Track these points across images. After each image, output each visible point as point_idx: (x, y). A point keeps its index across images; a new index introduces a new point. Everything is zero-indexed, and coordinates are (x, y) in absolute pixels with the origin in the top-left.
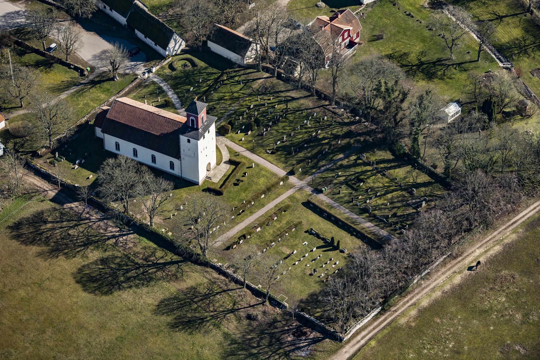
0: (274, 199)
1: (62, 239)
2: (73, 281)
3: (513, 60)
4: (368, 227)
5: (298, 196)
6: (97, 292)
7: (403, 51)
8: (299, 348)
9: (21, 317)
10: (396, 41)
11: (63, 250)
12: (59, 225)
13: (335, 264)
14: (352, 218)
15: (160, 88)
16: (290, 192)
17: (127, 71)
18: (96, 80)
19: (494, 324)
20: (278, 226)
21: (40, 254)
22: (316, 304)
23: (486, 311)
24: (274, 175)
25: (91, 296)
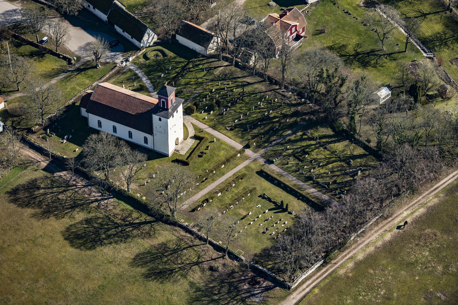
1: (53, 202)
2: (62, 238)
3: (435, 51)
4: (312, 193)
5: (253, 166)
6: (82, 247)
7: (342, 43)
8: (254, 295)
10: (336, 35)
11: (53, 212)
12: (50, 191)
15: (136, 75)
16: (246, 163)
17: (108, 60)
18: (82, 67)
19: (419, 275)
20: (236, 191)
21: (34, 216)
22: (268, 258)
23: (412, 264)
24: (233, 148)
25: (77, 251)
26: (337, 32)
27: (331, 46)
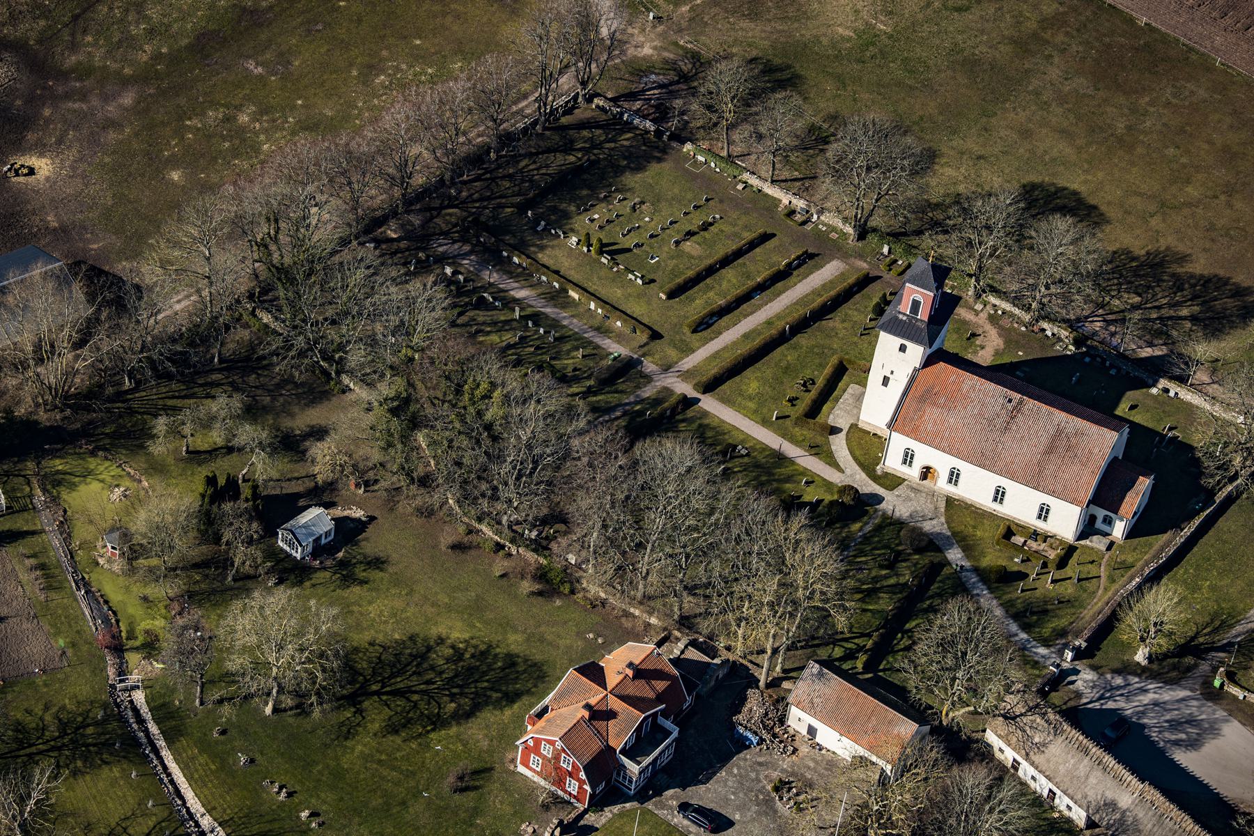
0: (723, 349)
1: (1149, 287)
2: (1103, 208)
3: (105, 706)
4: (522, 288)
5: (672, 353)
6: (1053, 189)
7: (398, 740)
8: (661, 86)
9: (1178, 152)
10: (413, 773)
11: (1141, 265)
12: (1165, 312)
13: (592, 220)
14: (555, 306)
15: (1026, 627)
16: (689, 362)
17: (1119, 681)
18: (1189, 660)
19: (294, 107)
20: (711, 294)
21: (1183, 259)
22: (631, 154)
23: (306, 129)
24: (726, 401)
25: (1062, 183)
26: (412, 784)
27: (433, 730)
